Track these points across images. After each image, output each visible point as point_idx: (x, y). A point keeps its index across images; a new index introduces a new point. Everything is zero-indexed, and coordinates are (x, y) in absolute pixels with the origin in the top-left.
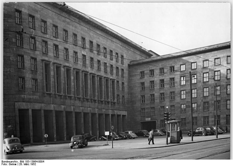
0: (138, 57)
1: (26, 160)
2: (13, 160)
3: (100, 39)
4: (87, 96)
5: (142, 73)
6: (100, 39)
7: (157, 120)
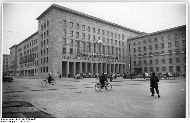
0: (134, 36)
1: (21, 118)
2: (11, 118)
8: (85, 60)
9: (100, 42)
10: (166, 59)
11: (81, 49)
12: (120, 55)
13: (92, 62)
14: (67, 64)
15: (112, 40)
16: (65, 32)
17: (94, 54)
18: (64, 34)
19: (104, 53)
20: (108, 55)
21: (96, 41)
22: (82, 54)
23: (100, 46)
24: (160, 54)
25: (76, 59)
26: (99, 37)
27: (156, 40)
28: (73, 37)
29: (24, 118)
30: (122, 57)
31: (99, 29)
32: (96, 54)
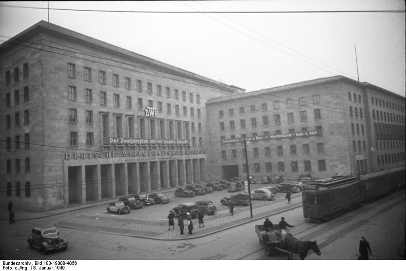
0: (217, 94)
2: (23, 261)
5: (221, 113)
8: (123, 158)
9: (153, 114)
10: (284, 147)
11: (112, 131)
12: (194, 138)
13: (138, 160)
14: (81, 170)
16: (73, 92)
17: (141, 142)
18: (70, 98)
19: (162, 137)
20: (171, 141)
21: (145, 111)
22: (113, 144)
23: (152, 121)
24: (274, 135)
25: (101, 157)
26: (151, 102)
27: (264, 106)
28: (94, 105)
29: (52, 261)
30: (197, 142)
31: (150, 82)
32: (146, 141)
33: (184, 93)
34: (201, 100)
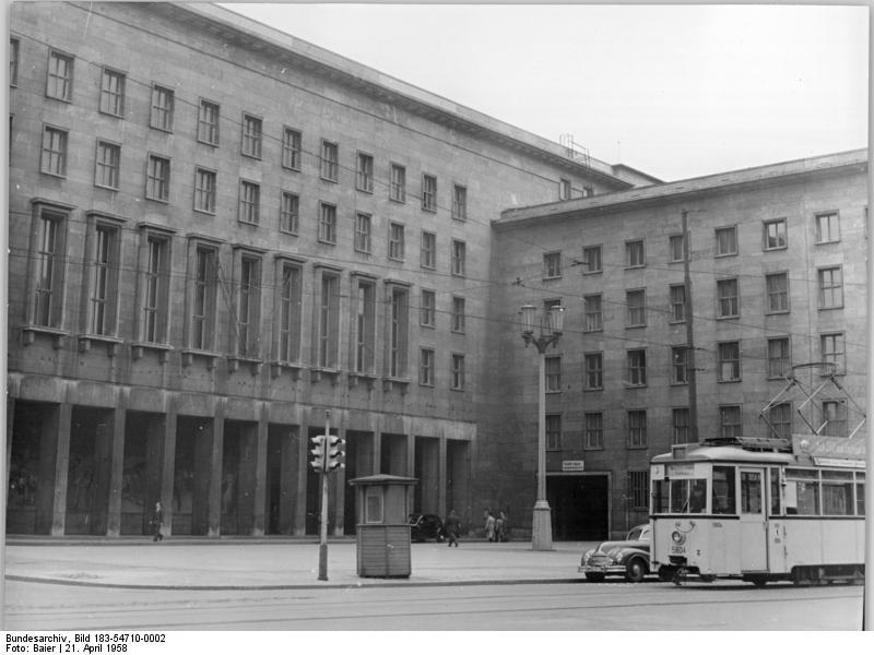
0: (539, 193)
1: (99, 633)
3: (339, 122)
4: (370, 362)
6: (339, 122)
7: (610, 470)
15: (366, 218)
16: (56, 147)
33: (366, 160)
34: (470, 208)
